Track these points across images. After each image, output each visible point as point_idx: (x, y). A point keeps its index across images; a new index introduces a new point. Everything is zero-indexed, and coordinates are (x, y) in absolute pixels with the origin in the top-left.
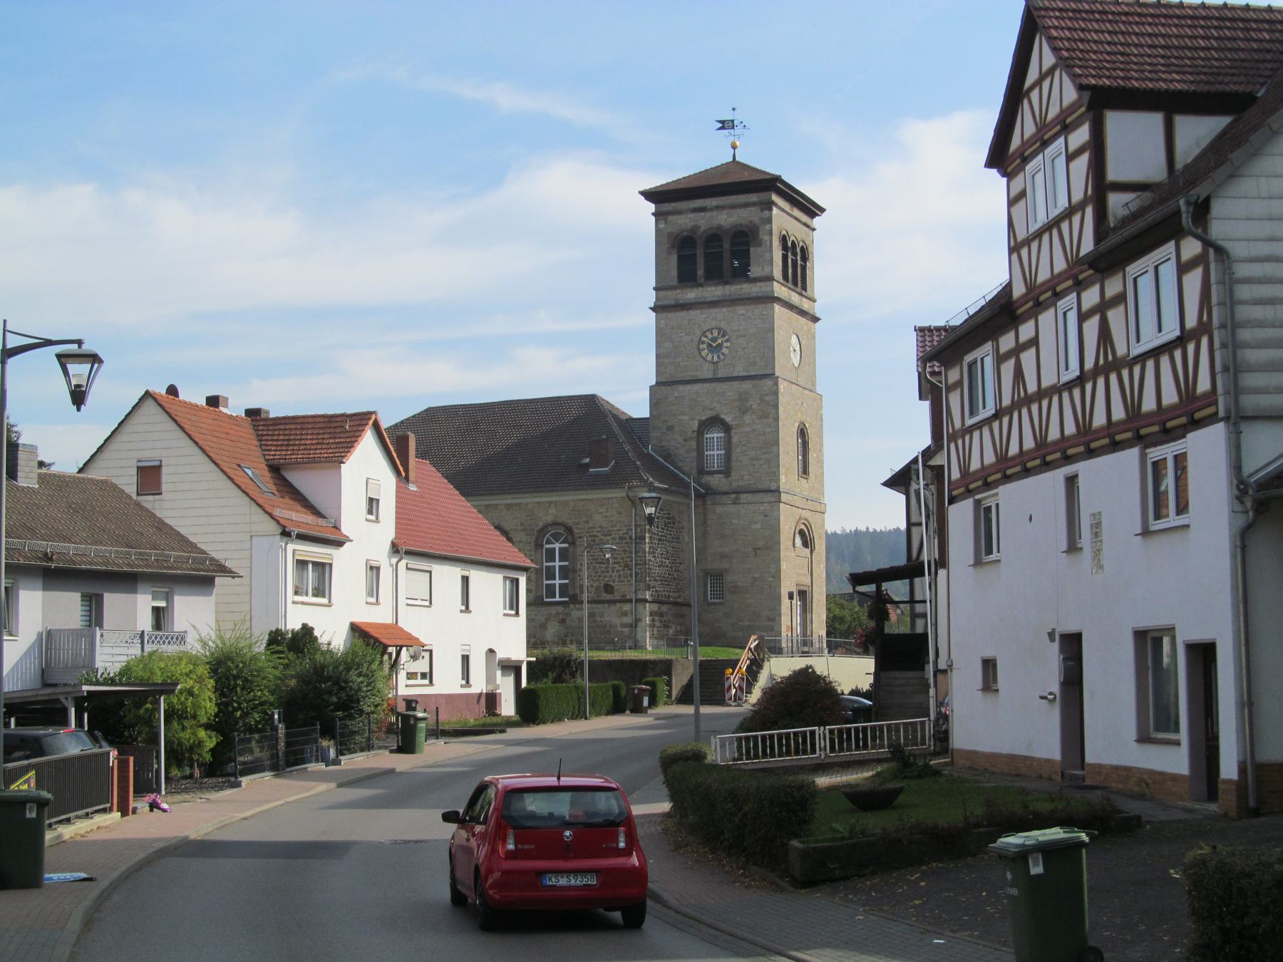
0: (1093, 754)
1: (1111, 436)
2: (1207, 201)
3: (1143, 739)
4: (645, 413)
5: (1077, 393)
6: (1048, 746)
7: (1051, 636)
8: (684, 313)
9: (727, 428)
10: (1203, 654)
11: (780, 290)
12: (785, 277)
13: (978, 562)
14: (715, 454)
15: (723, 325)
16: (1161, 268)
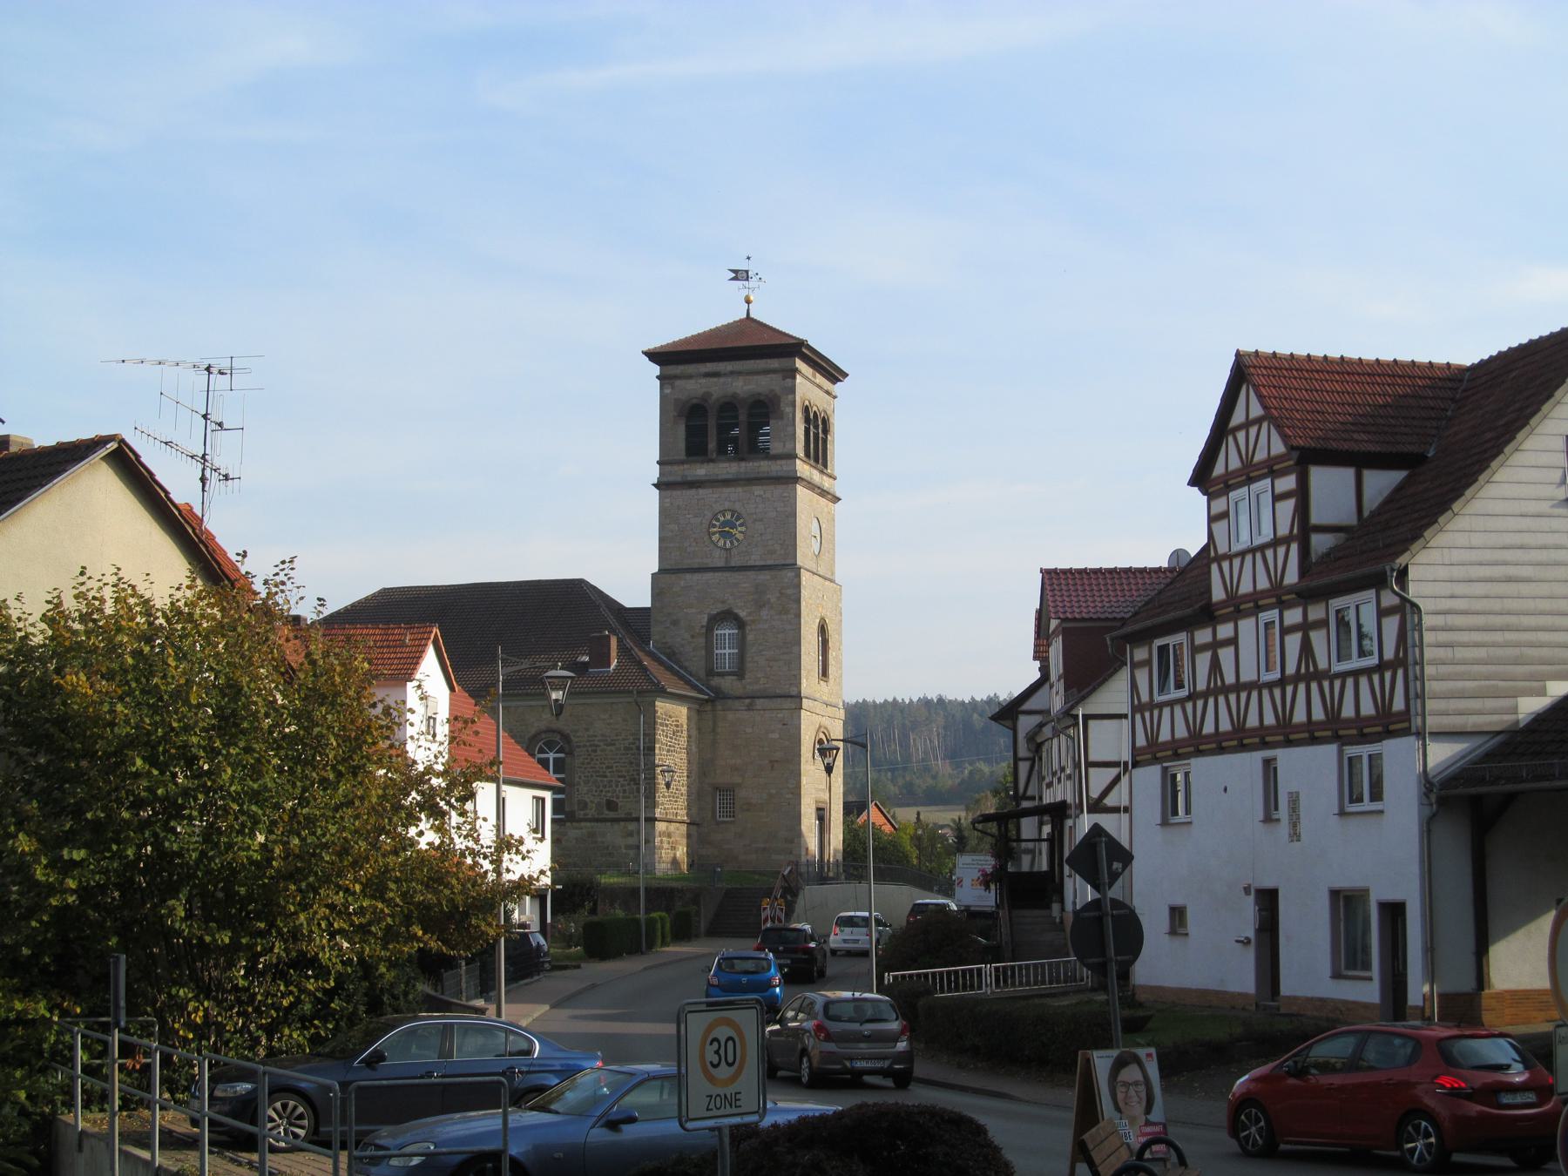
0: (1290, 985)
1: (1311, 733)
2: (1406, 567)
3: (1336, 975)
4: (644, 601)
5: (1277, 692)
6: (1241, 977)
7: (1247, 890)
8: (693, 492)
9: (741, 624)
10: (1394, 912)
11: (803, 468)
12: (807, 454)
13: (1165, 823)
14: (726, 652)
15: (738, 507)
16: (1362, 608)
